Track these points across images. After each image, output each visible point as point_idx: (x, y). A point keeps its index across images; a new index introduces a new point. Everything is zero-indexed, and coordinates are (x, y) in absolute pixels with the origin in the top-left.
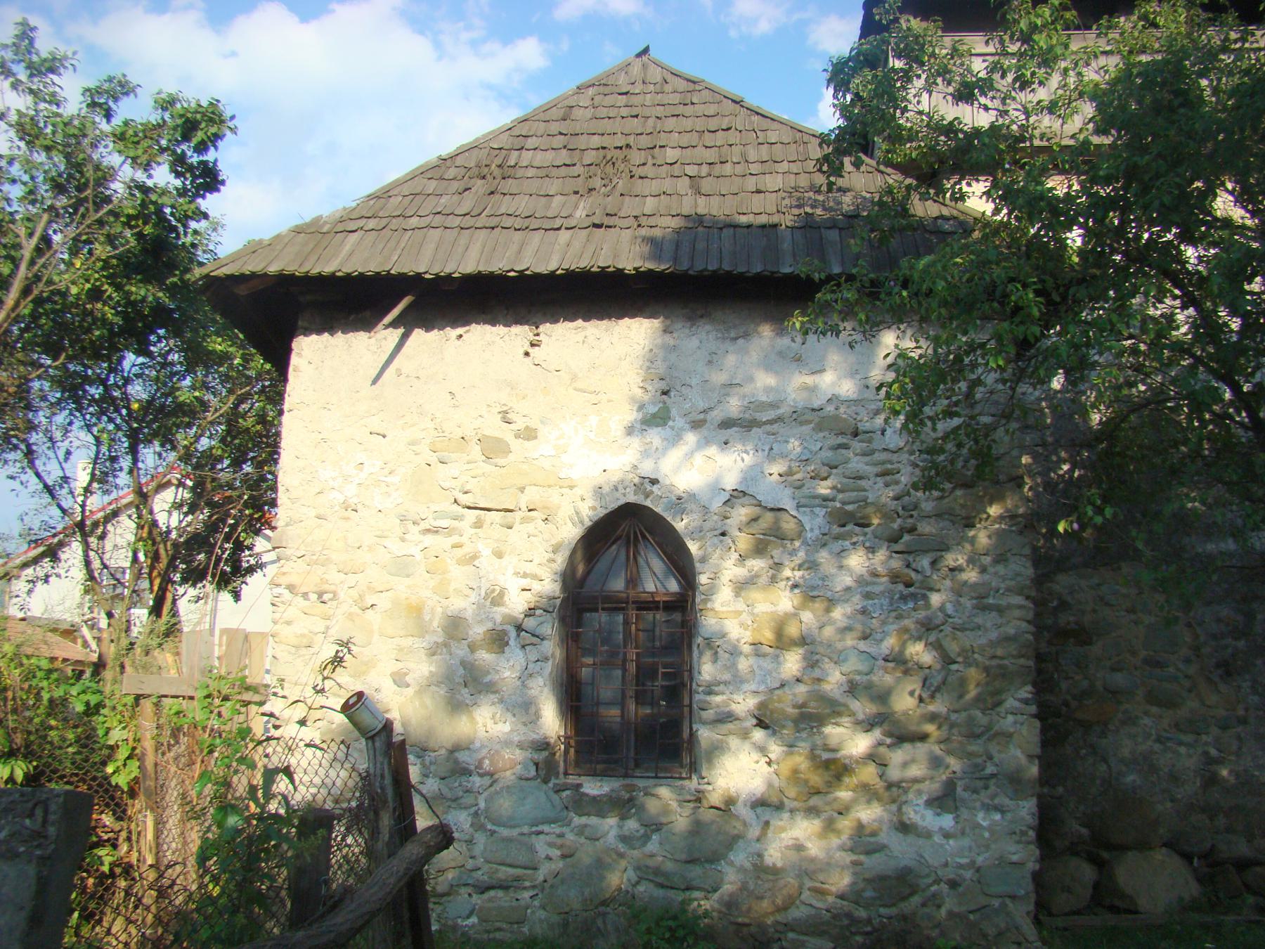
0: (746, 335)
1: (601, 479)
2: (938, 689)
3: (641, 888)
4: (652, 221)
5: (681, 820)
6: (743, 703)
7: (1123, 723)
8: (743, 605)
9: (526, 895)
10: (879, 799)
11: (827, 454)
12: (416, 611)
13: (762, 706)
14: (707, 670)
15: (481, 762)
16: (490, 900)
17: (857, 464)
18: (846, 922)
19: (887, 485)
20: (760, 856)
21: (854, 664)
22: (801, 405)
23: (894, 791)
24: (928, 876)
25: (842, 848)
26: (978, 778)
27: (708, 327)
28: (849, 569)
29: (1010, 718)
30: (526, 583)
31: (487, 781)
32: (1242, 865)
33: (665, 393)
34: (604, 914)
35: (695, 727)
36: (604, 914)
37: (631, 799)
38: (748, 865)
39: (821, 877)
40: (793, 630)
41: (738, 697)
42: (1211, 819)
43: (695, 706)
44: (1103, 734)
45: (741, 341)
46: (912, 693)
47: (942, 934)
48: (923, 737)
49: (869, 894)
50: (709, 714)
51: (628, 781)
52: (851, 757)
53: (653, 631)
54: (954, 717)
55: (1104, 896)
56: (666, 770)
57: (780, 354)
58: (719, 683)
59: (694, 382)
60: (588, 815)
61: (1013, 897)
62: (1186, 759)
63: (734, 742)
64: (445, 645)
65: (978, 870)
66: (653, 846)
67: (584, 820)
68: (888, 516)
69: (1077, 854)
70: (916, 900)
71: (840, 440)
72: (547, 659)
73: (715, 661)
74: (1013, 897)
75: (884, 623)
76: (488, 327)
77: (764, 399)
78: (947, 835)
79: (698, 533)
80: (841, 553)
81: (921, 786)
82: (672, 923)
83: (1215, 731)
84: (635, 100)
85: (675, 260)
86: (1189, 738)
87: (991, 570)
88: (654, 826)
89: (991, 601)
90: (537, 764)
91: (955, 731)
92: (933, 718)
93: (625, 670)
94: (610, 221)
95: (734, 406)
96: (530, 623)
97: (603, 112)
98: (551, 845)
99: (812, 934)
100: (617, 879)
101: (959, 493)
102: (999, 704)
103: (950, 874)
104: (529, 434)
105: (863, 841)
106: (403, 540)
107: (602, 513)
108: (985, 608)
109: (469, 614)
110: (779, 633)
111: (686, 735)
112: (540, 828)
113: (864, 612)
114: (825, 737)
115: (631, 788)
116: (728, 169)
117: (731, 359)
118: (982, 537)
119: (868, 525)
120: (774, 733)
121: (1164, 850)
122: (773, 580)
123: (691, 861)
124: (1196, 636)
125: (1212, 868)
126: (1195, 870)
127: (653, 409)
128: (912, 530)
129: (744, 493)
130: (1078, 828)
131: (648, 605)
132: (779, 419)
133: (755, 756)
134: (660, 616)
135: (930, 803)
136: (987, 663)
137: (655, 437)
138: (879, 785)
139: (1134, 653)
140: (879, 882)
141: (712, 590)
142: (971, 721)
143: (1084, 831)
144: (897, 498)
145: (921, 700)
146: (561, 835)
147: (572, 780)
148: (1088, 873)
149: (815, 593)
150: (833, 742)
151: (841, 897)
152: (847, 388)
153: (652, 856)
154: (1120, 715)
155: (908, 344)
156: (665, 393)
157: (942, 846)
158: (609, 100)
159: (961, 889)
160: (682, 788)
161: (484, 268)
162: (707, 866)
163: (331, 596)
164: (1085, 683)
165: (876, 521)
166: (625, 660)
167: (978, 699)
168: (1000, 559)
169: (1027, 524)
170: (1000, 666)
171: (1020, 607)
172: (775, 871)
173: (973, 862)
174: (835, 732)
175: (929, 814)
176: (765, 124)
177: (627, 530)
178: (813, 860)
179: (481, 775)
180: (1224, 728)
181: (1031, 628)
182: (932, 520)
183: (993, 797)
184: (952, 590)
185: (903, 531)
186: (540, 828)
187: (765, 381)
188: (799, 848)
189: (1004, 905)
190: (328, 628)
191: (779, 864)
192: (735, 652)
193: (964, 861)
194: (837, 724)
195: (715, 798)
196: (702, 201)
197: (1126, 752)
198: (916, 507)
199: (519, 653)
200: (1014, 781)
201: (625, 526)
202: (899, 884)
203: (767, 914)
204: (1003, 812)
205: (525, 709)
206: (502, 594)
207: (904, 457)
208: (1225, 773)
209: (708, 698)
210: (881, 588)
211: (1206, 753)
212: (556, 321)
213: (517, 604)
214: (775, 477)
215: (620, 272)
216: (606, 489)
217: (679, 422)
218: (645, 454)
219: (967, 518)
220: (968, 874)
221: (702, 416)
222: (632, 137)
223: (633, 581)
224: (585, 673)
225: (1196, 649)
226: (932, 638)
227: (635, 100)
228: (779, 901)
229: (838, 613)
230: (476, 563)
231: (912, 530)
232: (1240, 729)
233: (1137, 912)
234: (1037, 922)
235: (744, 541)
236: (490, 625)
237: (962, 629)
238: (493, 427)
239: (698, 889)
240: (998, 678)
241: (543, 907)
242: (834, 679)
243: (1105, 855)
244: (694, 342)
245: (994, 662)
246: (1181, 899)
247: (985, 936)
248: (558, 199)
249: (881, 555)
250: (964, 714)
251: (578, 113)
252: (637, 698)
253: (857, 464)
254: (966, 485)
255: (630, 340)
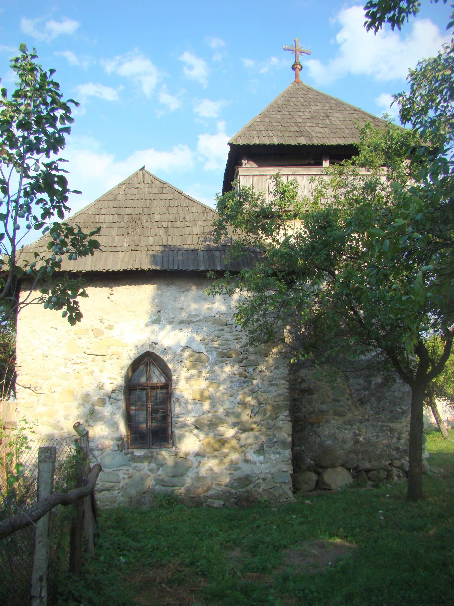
0: (187, 290)
1: (138, 343)
2: (257, 413)
3: (157, 487)
4: (153, 248)
5: (170, 461)
6: (190, 420)
7: (326, 423)
8: (188, 386)
9: (116, 492)
10: (238, 452)
11: (217, 332)
12: (72, 393)
13: (196, 421)
14: (177, 409)
15: (98, 445)
16: (103, 495)
17: (227, 336)
18: (228, 494)
19: (238, 343)
20: (198, 473)
21: (227, 405)
22: (207, 315)
23: (243, 448)
24: (255, 477)
25: (227, 469)
26: (272, 443)
27: (174, 288)
28: (225, 372)
29: (281, 422)
30: (111, 381)
31: (100, 452)
32: (368, 471)
33: (159, 312)
34: (144, 497)
35: (173, 430)
36: (144, 497)
37: (152, 456)
38: (194, 477)
39: (219, 479)
40: (206, 394)
41: (188, 418)
42: (357, 456)
43: (173, 423)
44: (318, 427)
45: (185, 293)
46: (248, 415)
47: (261, 496)
48: (252, 429)
49: (236, 484)
50: (179, 425)
51: (150, 450)
52: (228, 438)
53: (156, 396)
54: (262, 422)
55: (320, 485)
56: (163, 445)
57: (199, 297)
58: (181, 414)
59: (169, 308)
60: (137, 462)
61: (284, 483)
62: (348, 435)
63: (187, 434)
64: (83, 404)
65: (272, 474)
66: (160, 472)
67: (136, 464)
68: (238, 354)
69: (310, 471)
70: (252, 485)
71: (221, 327)
72: (120, 408)
73: (179, 407)
74: (284, 483)
75: (237, 391)
76: (94, 288)
77: (194, 313)
78: (261, 463)
79: (172, 360)
80: (222, 367)
81: (252, 447)
82: (168, 498)
83: (358, 424)
84: (142, 191)
85: (162, 265)
86: (349, 427)
87: (274, 371)
88: (161, 465)
89: (274, 382)
90: (118, 446)
91: (263, 427)
92: (255, 423)
93: (147, 411)
94: (138, 248)
95: (184, 316)
96: (113, 395)
97: (129, 197)
98: (124, 474)
99: (217, 499)
100: (150, 483)
101: (262, 345)
102: (277, 417)
103: (262, 476)
104: (110, 327)
105: (233, 466)
106: (66, 367)
107: (138, 355)
108: (272, 385)
109: (91, 393)
110: (202, 394)
111: (170, 432)
112: (120, 468)
113: (231, 387)
114: (219, 431)
115: (152, 452)
116: (178, 224)
117: (182, 298)
118: (270, 360)
119: (231, 357)
120: (201, 430)
121: (341, 467)
122: (199, 377)
123: (174, 476)
124: (351, 390)
125: (358, 473)
126: (352, 474)
127: (154, 318)
128: (247, 358)
129: (188, 347)
130: (307, 461)
131: (154, 387)
132: (200, 320)
133: (195, 438)
134: (159, 391)
135: (255, 452)
136: (273, 403)
137: (156, 327)
138: (238, 446)
139: (329, 397)
140: (239, 480)
141: (177, 382)
142: (268, 423)
143: (312, 462)
144: (241, 348)
145: (251, 417)
146: (128, 470)
147: (130, 450)
148: (314, 477)
149: (213, 381)
150: (221, 432)
151: (226, 486)
152: (223, 308)
153: (160, 475)
154: (324, 420)
155: (245, 293)
156: (159, 312)
157: (260, 467)
158: (131, 191)
159: (266, 481)
160: (170, 451)
161: (94, 269)
162: (180, 478)
163: (39, 388)
164: (311, 409)
165: (234, 356)
166: (147, 407)
167: (271, 416)
168: (277, 368)
169: (284, 356)
170: (277, 405)
171: (284, 384)
172: (203, 478)
173: (270, 472)
174: (221, 429)
175: (255, 456)
176: (192, 204)
177: (147, 360)
178: (216, 473)
179: (98, 451)
180: (361, 423)
181: (288, 391)
182: (253, 355)
183: (276, 449)
184: (261, 379)
185: (243, 359)
186: (120, 468)
187: (194, 306)
188: (211, 470)
189: (281, 486)
190: (38, 400)
191: (204, 476)
192: (187, 402)
193: (267, 471)
194: (223, 427)
195: (181, 454)
196: (170, 238)
197: (326, 433)
198: (248, 350)
199: (110, 406)
200: (283, 443)
201: (146, 359)
202: (246, 480)
203: (201, 494)
204: (280, 454)
205: (115, 426)
206: (103, 385)
207: (244, 333)
208: (361, 439)
209: (178, 419)
210: (236, 379)
211: (354, 432)
212: (119, 286)
213: (109, 388)
214: (199, 341)
215: (143, 270)
216: (139, 347)
217: (164, 322)
218: (153, 332)
219: (265, 354)
220: (269, 476)
221: (172, 320)
222: (142, 209)
223: (149, 378)
224: (133, 412)
225: (351, 395)
226: (254, 396)
227: (142, 191)
228: (205, 488)
229: (222, 388)
230: (93, 374)
231: (247, 358)
232: (366, 423)
233: (331, 490)
234: (294, 493)
235: (188, 363)
236: (99, 397)
237: (264, 392)
238: (97, 325)
239: (177, 486)
240: (277, 409)
241: (122, 496)
242: (221, 411)
243: (320, 470)
244: (169, 294)
245: (276, 403)
246: (346, 484)
247: (275, 496)
248: (116, 237)
249: (236, 367)
250: (266, 421)
251: (120, 197)
252: (152, 420)
253: (227, 336)
254: (264, 342)
255: (147, 291)
